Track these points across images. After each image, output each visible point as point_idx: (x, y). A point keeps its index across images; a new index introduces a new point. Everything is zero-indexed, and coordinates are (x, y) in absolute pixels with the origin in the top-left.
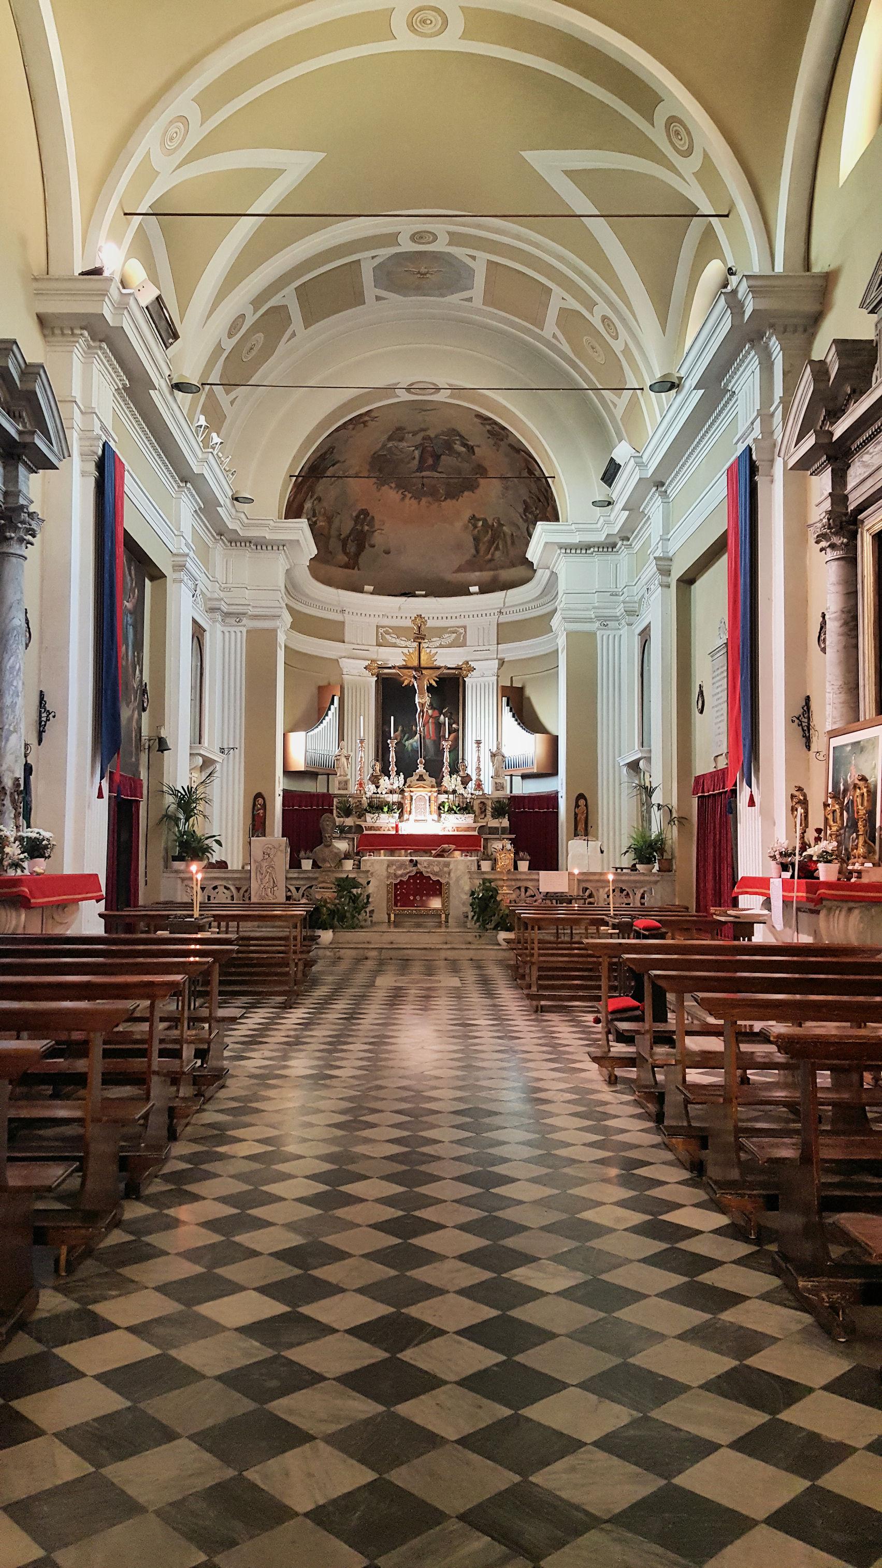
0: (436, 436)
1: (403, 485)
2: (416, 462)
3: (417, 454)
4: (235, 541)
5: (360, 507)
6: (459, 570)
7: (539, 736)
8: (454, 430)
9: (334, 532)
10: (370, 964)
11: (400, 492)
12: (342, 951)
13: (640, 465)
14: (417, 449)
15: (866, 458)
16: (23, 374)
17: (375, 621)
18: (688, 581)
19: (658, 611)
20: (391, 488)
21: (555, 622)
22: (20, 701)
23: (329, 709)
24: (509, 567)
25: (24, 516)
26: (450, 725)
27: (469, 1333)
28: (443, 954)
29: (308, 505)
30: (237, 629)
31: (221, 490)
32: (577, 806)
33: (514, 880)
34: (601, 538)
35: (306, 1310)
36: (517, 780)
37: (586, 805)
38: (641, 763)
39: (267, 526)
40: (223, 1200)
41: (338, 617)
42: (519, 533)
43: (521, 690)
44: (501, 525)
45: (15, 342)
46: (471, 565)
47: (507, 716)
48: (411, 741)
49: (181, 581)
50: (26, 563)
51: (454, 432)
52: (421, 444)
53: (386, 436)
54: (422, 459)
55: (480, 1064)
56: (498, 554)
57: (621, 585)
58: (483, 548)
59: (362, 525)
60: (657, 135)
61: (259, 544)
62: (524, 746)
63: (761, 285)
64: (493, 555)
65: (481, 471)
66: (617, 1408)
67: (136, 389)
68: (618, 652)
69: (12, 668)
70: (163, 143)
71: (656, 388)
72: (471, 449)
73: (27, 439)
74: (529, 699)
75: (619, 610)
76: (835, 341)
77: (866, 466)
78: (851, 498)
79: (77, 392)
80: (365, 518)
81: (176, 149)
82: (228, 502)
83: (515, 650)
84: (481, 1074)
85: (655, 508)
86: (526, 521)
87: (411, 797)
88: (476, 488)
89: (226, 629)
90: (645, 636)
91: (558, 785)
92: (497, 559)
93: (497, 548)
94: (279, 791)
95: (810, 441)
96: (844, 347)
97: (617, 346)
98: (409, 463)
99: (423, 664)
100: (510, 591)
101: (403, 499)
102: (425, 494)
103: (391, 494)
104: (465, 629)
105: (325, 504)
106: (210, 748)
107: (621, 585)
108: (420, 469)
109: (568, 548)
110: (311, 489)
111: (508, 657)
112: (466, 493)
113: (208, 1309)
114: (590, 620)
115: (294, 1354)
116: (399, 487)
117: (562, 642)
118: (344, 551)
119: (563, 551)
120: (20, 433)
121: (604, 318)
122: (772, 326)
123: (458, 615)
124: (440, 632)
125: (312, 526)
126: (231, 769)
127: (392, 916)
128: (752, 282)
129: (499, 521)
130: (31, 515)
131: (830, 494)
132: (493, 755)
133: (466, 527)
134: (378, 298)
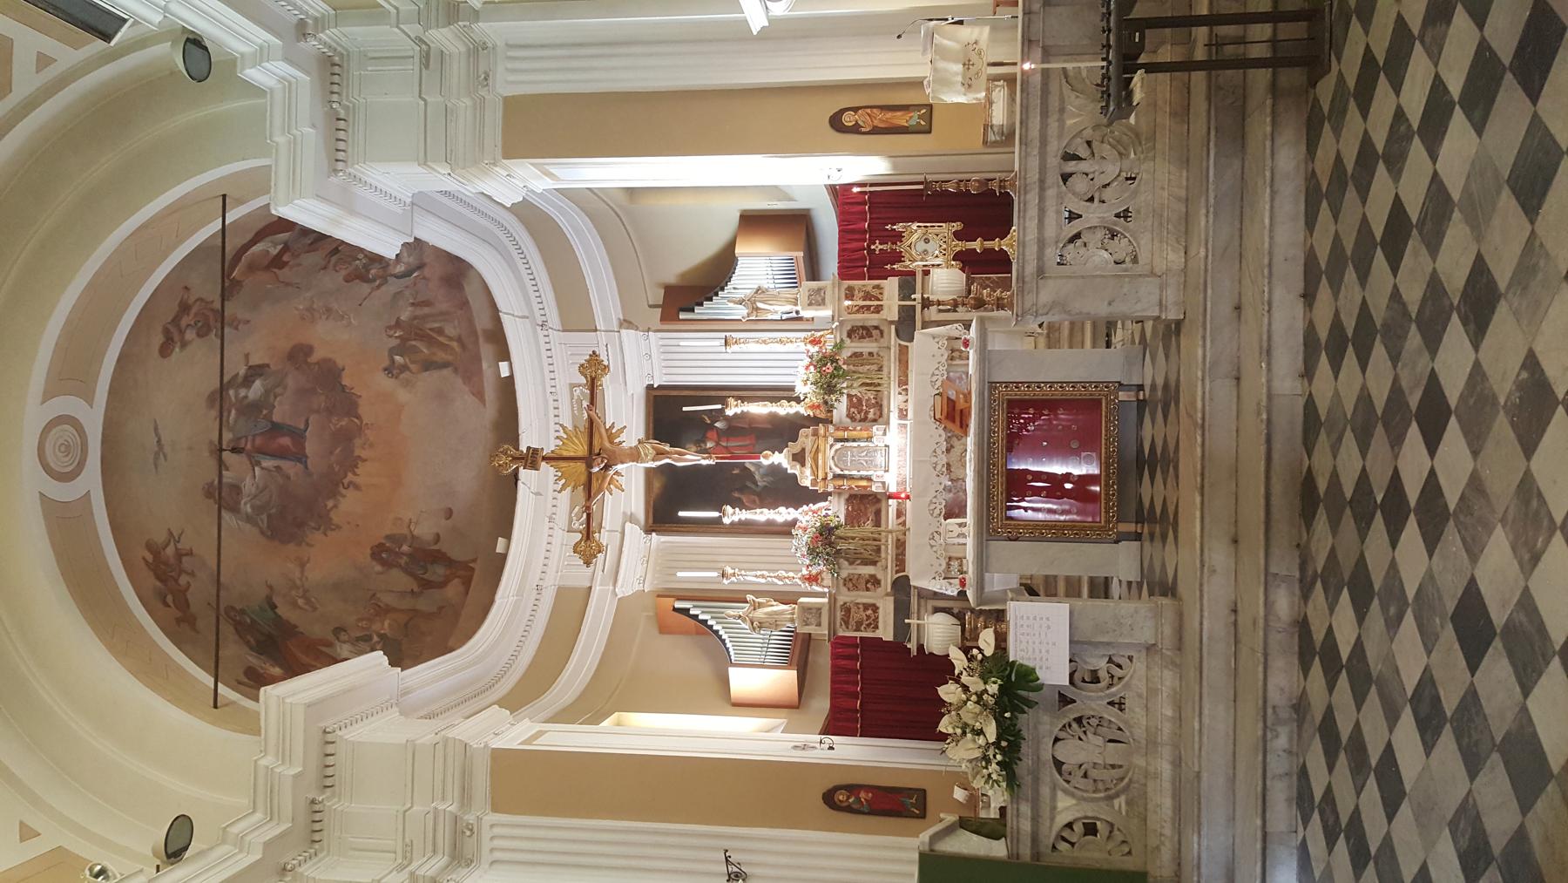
1: (333, 485)
2: (288, 466)
3: (268, 463)
5: (364, 557)
6: (479, 395)
8: (211, 399)
9: (407, 603)
12: (1275, 697)
14: (258, 463)
20: (335, 506)
23: (695, 617)
27: (1432, 445)
30: (486, 834)
32: (856, 129)
33: (1042, 189)
37: (855, 110)
40: (1331, 687)
43: (670, 290)
44: (398, 324)
46: (470, 372)
48: (757, 477)
52: (250, 457)
54: (281, 454)
56: (450, 330)
58: (441, 356)
64: (451, 339)
74: (683, 275)
80: (388, 550)
83: (605, 301)
86: (385, 280)
87: (836, 477)
93: (440, 331)
99: (582, 450)
101: (357, 487)
103: (348, 505)
111: (616, 313)
112: (346, 381)
113: (1345, 652)
116: (334, 494)
118: (443, 585)
119: (340, 165)
123: (551, 398)
126: (771, 859)
127: (1123, 527)
129: (390, 328)
133: (407, 384)
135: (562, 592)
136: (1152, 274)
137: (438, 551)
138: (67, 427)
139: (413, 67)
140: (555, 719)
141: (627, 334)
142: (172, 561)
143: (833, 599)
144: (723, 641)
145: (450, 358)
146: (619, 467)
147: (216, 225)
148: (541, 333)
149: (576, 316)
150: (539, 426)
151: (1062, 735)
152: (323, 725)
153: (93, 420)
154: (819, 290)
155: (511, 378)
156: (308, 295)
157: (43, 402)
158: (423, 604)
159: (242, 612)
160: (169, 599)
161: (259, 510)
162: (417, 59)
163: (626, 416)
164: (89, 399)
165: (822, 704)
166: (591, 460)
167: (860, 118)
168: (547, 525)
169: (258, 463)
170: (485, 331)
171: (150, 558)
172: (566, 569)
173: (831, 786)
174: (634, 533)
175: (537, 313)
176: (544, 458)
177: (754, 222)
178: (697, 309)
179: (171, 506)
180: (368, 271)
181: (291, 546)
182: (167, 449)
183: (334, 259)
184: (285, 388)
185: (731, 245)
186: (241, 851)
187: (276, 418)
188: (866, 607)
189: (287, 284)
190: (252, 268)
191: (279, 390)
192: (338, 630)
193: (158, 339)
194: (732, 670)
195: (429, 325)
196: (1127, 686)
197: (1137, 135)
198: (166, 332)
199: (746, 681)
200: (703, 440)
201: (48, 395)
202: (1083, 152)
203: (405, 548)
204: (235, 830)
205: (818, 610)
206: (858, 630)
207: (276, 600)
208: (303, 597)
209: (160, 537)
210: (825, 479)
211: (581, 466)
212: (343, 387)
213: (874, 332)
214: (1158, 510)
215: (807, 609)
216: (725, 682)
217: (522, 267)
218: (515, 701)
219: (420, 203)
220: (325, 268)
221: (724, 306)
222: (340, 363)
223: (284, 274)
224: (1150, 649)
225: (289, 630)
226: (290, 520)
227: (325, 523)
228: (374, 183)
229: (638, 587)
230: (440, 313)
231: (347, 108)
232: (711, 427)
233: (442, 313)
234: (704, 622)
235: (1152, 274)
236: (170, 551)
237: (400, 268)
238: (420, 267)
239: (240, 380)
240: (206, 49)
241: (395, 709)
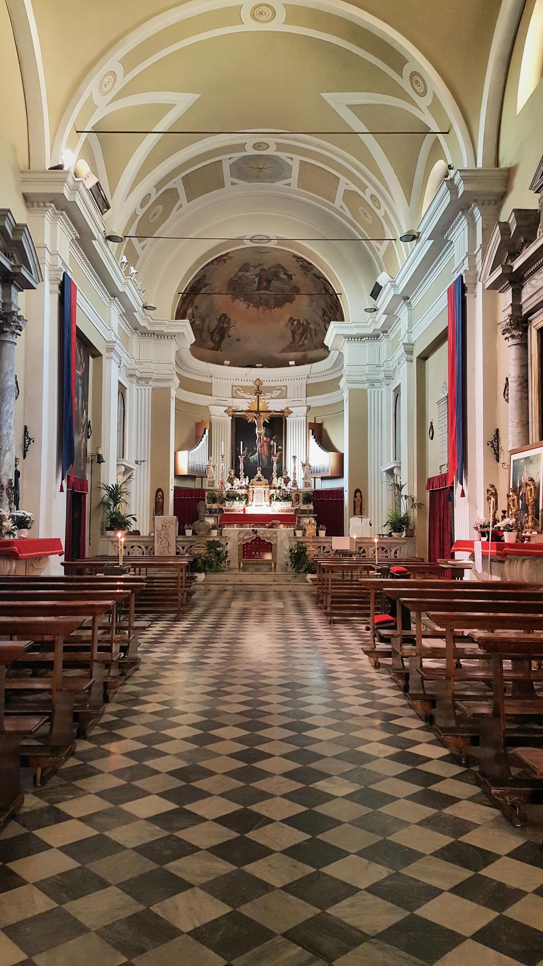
0: (269, 269)
1: (248, 299)
2: (256, 284)
3: (257, 279)
4: (145, 333)
5: (221, 312)
8: (279, 265)
9: (205, 328)
10: (228, 594)
11: (246, 303)
13: (394, 286)
14: (257, 276)
15: (533, 282)
16: (14, 230)
17: (231, 383)
18: (423, 358)
19: (405, 376)
20: (241, 300)
21: (342, 383)
22: (12, 432)
23: (203, 437)
24: (313, 349)
25: (15, 318)
26: (277, 446)
27: (289, 821)
28: (273, 588)
29: (189, 311)
30: (146, 388)
31: (136, 301)
32: (355, 496)
34: (370, 331)
35: (189, 807)
36: (318, 481)
37: (361, 496)
38: (395, 470)
39: (164, 324)
40: (137, 739)
41: (208, 380)
42: (319, 328)
43: (321, 425)
45: (9, 211)
46: (291, 348)
48: (253, 457)
49: (112, 358)
50: (16, 347)
51: (280, 266)
52: (259, 274)
54: (260, 283)
55: (296, 656)
56: (306, 341)
57: (383, 360)
59: (223, 323)
60: (405, 83)
61: (159, 335)
62: (322, 460)
63: (469, 176)
64: (303, 342)
65: (296, 290)
66: (380, 867)
67: (83, 239)
68: (381, 401)
69: (8, 411)
70: (100, 88)
71: (404, 239)
72: (290, 277)
73: (17, 270)
74: (326, 430)
75: (381, 376)
76: (514, 210)
77: (534, 287)
78: (524, 306)
79: (47, 242)
80: (225, 319)
81: (108, 92)
82: (140, 309)
83: (317, 401)
84: (296, 661)
85: (403, 313)
86: (324, 321)
87: (253, 491)
89: (139, 388)
90: (397, 392)
91: (344, 483)
92: (306, 344)
93: (306, 338)
94: (172, 487)
95: (499, 272)
96: (520, 213)
97: (380, 213)
98: (251, 285)
102: (261, 304)
103: (241, 305)
104: (286, 387)
105: (200, 310)
106: (129, 460)
107: (383, 360)
108: (259, 289)
109: (350, 338)
110: (192, 301)
111: (313, 405)
112: (287, 304)
114: (363, 382)
115: (181, 834)
116: (245, 300)
117: (346, 395)
118: (212, 339)
119: (347, 339)
120: (12, 267)
121: (372, 196)
122: (475, 201)
123: (282, 379)
124: (271, 389)
125: (192, 324)
127: (242, 564)
128: (463, 174)
130: (19, 317)
131: (511, 304)
132: (304, 465)
133: (287, 325)
134: (233, 184)
148: (305, 377)
163: (275, 405)
167: (359, 497)
186: (71, 190)
191: (283, 283)
195: (308, 334)
202: (325, 551)
206: (208, 498)
212: (285, 303)
217: (328, 372)
227: (235, 297)
232: (272, 439)
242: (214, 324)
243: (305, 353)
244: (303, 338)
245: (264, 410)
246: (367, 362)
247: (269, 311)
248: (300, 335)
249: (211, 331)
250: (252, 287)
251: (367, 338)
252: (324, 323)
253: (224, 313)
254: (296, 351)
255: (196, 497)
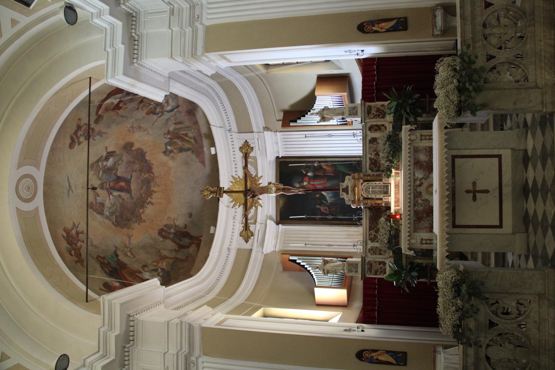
0: (100, 179)
1: (142, 203)
2: (123, 194)
3: (116, 193)
6: (203, 162)
7: (316, 93)
9: (172, 255)
11: (147, 206)
14: (111, 194)
23: (299, 264)
24: (198, 126)
39: (105, 333)
42: (172, 118)
43: (286, 113)
44: (169, 132)
46: (198, 152)
47: (302, 121)
48: (328, 198)
52: (107, 190)
53: (98, 216)
54: (121, 189)
56: (190, 135)
58: (187, 146)
59: (170, 233)
64: (191, 138)
65: (128, 146)
74: (292, 106)
80: (165, 231)
83: (257, 119)
86: (162, 113)
88: (143, 151)
93: (186, 135)
98: (124, 200)
100: (211, 122)
101: (152, 204)
102: (148, 188)
103: (149, 210)
105: (149, 262)
111: (262, 124)
112: (148, 158)
114: (195, 32)
116: (142, 207)
118: (188, 247)
119: (135, 61)
133: (173, 158)
135: (239, 251)
136: (537, 87)
137: (186, 232)
138: (29, 179)
139: (166, 16)
140: (231, 312)
141: (267, 134)
142: (75, 236)
143: (363, 259)
144: (312, 275)
145: (190, 146)
146: (260, 197)
147: (86, 93)
148: (229, 134)
149: (244, 126)
150: (229, 173)
151: (491, 343)
152: (128, 313)
153: (40, 176)
154: (354, 107)
155: (216, 154)
156: (132, 120)
157: (17, 169)
158: (180, 256)
159: (104, 258)
160: (73, 252)
161: (112, 213)
162: (168, 12)
163: (267, 174)
164: (38, 167)
165: (358, 304)
166: (249, 193)
168: (232, 221)
169: (111, 194)
170: (205, 134)
171: (65, 235)
172: (238, 242)
173: (363, 348)
174: (271, 225)
175: (227, 125)
176: (225, 192)
177: (323, 79)
178: (298, 121)
179: (73, 211)
180: (155, 110)
181: (125, 230)
182: (73, 188)
183: (141, 105)
184: (122, 161)
185: (313, 91)
187: (119, 174)
188: (380, 263)
189: (122, 117)
190: (107, 110)
191: (120, 162)
192: (145, 266)
193: (68, 141)
194: (316, 290)
196: (528, 316)
197: (524, 13)
198: (72, 138)
199: (322, 294)
200: (302, 181)
201: (20, 165)
203: (172, 230)
204: (89, 360)
205: (355, 265)
206: (376, 274)
207: (119, 253)
208: (130, 251)
209: (69, 226)
210: (359, 200)
211: (242, 195)
213: (382, 128)
214: (540, 218)
215: (351, 264)
216: (313, 293)
217: (220, 105)
218: (214, 304)
219: (172, 77)
220: (138, 109)
221: (312, 119)
222: (145, 150)
223: (121, 112)
224: (541, 296)
225: (123, 266)
226: (124, 218)
227: (140, 220)
228: (149, 67)
229: (272, 249)
230: (185, 126)
231: (138, 35)
232: (306, 175)
233: (187, 127)
234: (303, 266)
235: (537, 87)
236: (74, 232)
237: (169, 108)
238: (178, 107)
239: (104, 158)
240: (75, 11)
241: (162, 305)
242: (170, 244)
243: (203, 135)
244: (187, 138)
245: (243, 182)
246: (165, 30)
247: (157, 180)
248: (183, 143)
249: (177, 249)
250: (126, 200)
251: (133, 31)
252: (165, 113)
253: (157, 232)
254: (203, 147)
255: (375, 289)
